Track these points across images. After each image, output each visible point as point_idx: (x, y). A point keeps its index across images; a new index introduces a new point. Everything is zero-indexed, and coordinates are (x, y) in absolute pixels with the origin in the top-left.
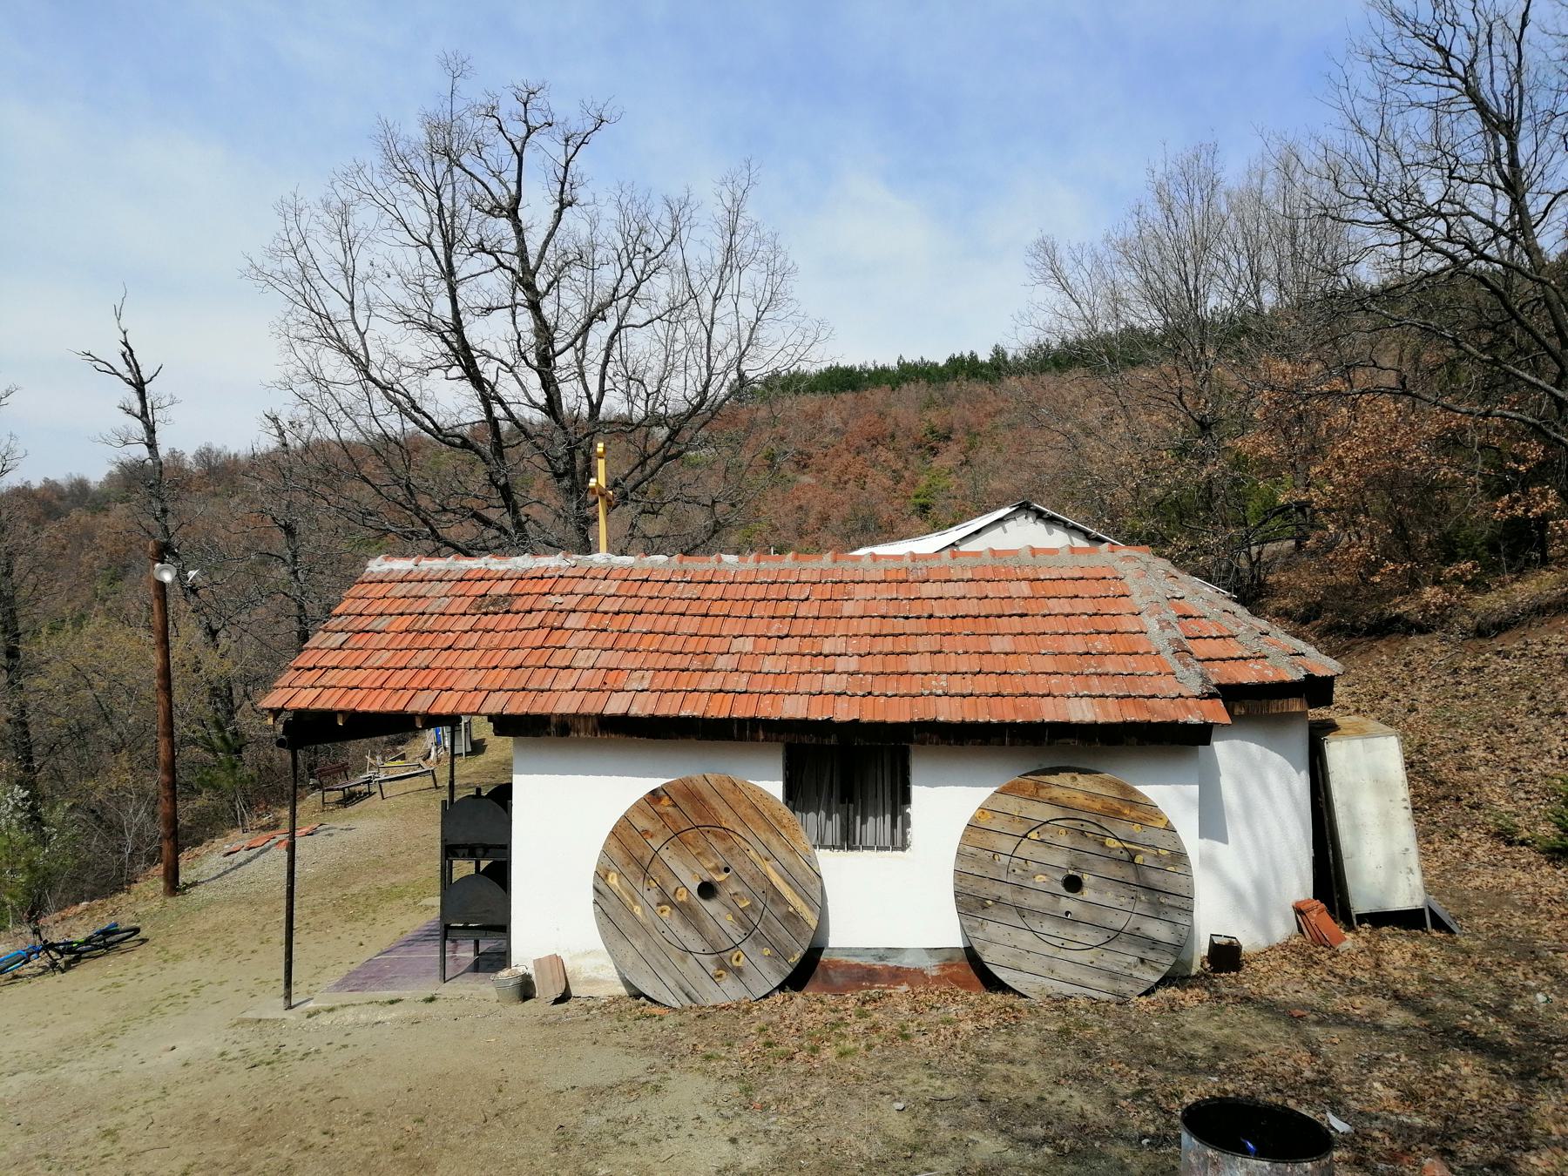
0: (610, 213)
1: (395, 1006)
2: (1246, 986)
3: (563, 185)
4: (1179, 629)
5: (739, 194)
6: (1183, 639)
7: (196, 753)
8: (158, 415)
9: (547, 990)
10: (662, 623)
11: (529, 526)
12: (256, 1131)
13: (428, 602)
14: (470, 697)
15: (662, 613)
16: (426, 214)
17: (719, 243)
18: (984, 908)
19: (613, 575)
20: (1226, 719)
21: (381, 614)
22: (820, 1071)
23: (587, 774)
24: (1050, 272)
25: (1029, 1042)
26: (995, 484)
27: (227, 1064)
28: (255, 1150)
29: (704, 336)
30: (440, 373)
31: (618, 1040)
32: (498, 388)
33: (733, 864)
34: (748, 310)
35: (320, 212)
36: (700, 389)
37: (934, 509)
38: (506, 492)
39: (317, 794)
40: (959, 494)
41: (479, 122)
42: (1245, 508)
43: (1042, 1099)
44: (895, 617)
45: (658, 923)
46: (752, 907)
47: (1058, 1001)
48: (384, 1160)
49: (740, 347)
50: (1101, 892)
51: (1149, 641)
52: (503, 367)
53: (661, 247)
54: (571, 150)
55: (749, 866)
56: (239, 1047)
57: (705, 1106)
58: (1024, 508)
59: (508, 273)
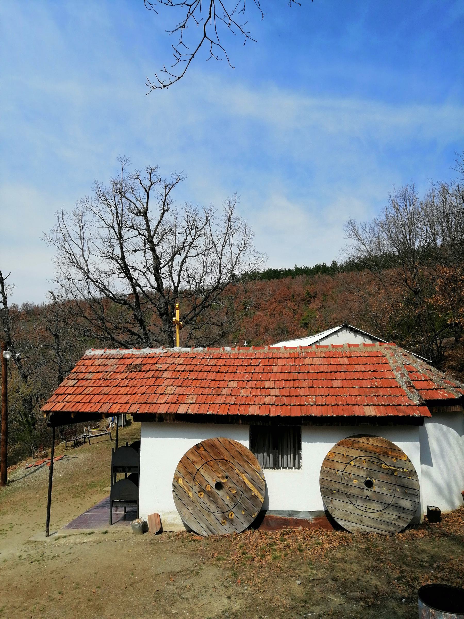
0: (182, 214)
1: (91, 535)
2: (444, 528)
3: (164, 203)
4: (408, 377)
5: (232, 206)
6: (411, 381)
7: (16, 425)
8: (8, 292)
9: (153, 529)
10: (200, 375)
11: (150, 335)
12: (31, 592)
13: (109, 367)
14: (124, 406)
15: (201, 371)
16: (112, 216)
17: (224, 225)
18: (332, 494)
19: (182, 356)
20: (429, 415)
21: (90, 372)
22: (266, 566)
23: (175, 438)
24: (353, 233)
25: (353, 554)
26: (334, 316)
27: (21, 561)
28: (30, 600)
29: (219, 260)
30: (116, 275)
31: (182, 551)
32: (138, 281)
33: (229, 475)
34: (235, 250)
35: (72, 215)
36: (217, 280)
37: (310, 325)
38: (141, 322)
39: (64, 442)
40: (320, 319)
41: (132, 181)
42: (434, 325)
43: (359, 580)
44: (294, 373)
45: (199, 500)
46: (237, 493)
47: (364, 535)
48: (84, 606)
49: (232, 264)
50: (381, 488)
51: (397, 382)
52: (141, 273)
53: (202, 226)
54: (167, 191)
55: (235, 476)
56: (26, 553)
57: (217, 581)
58: (345, 327)
59: (143, 237)
